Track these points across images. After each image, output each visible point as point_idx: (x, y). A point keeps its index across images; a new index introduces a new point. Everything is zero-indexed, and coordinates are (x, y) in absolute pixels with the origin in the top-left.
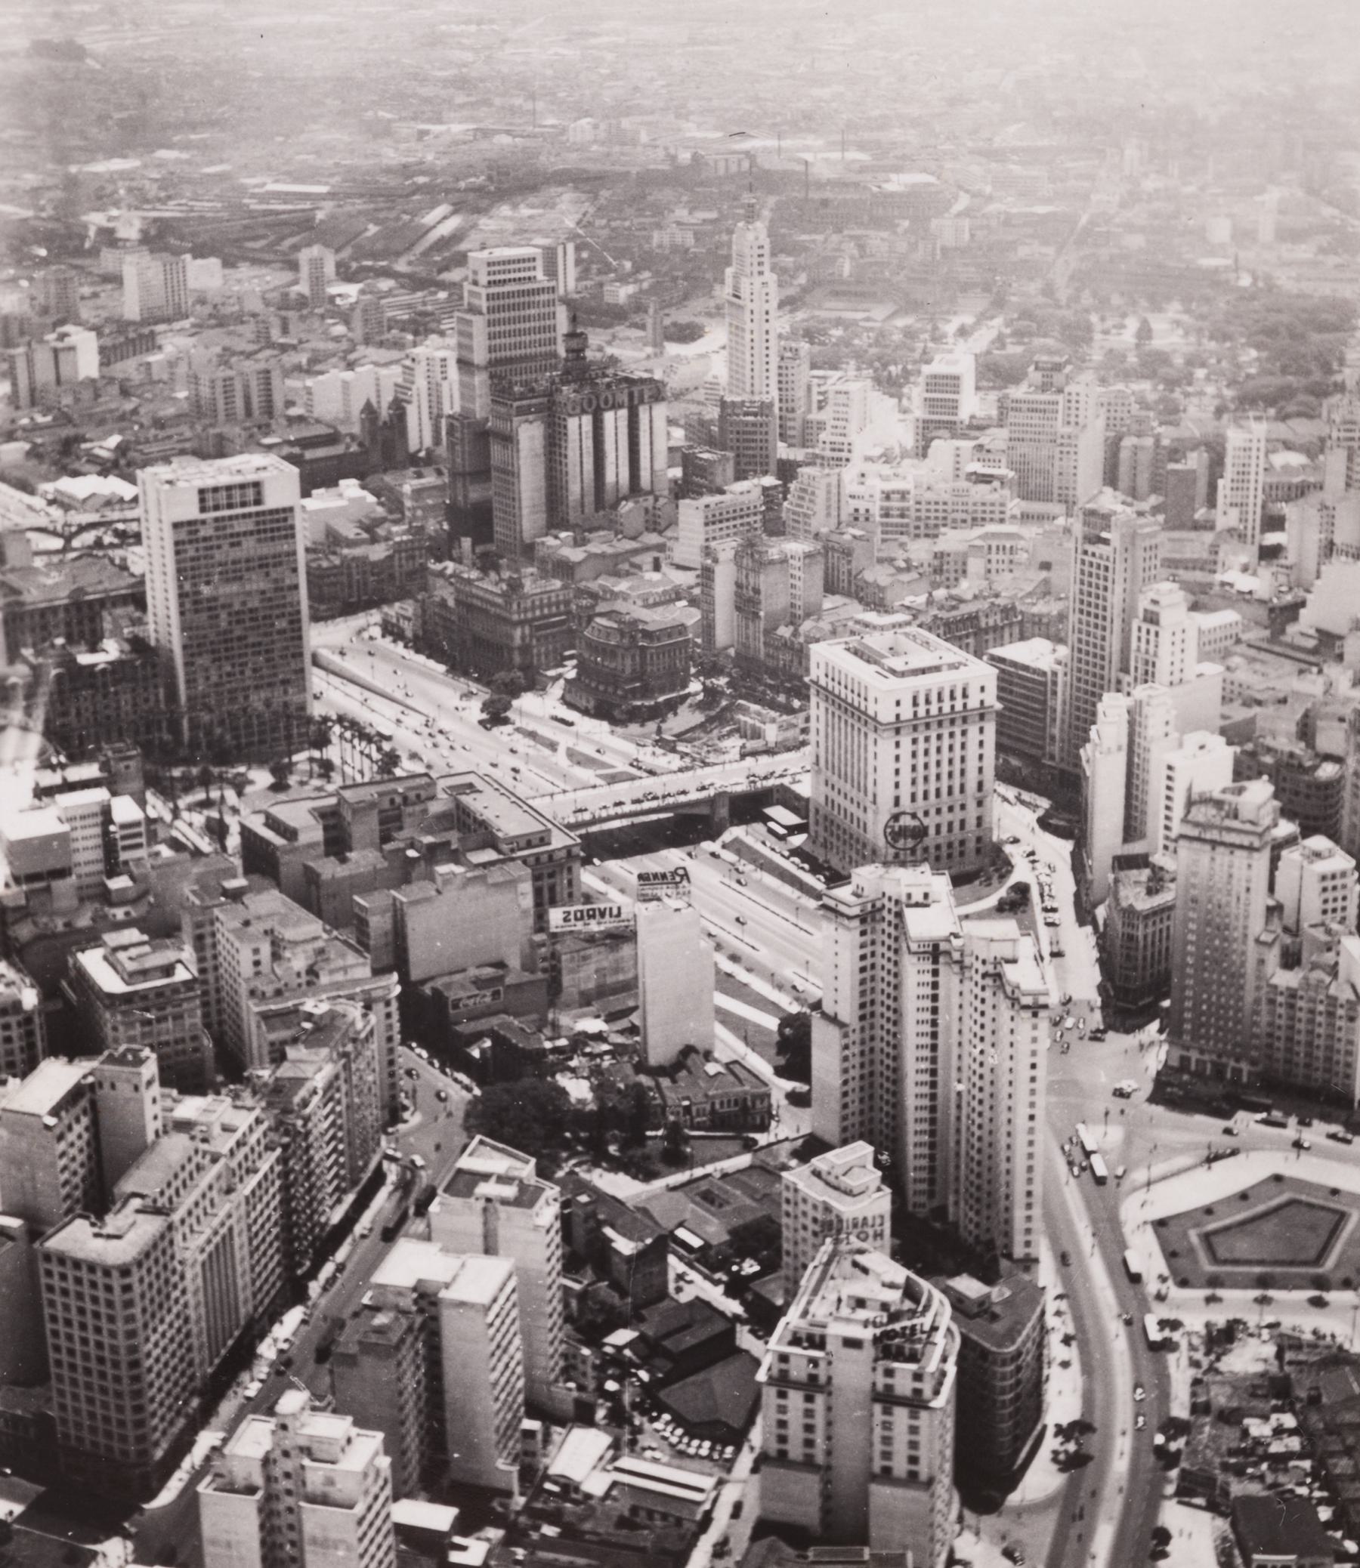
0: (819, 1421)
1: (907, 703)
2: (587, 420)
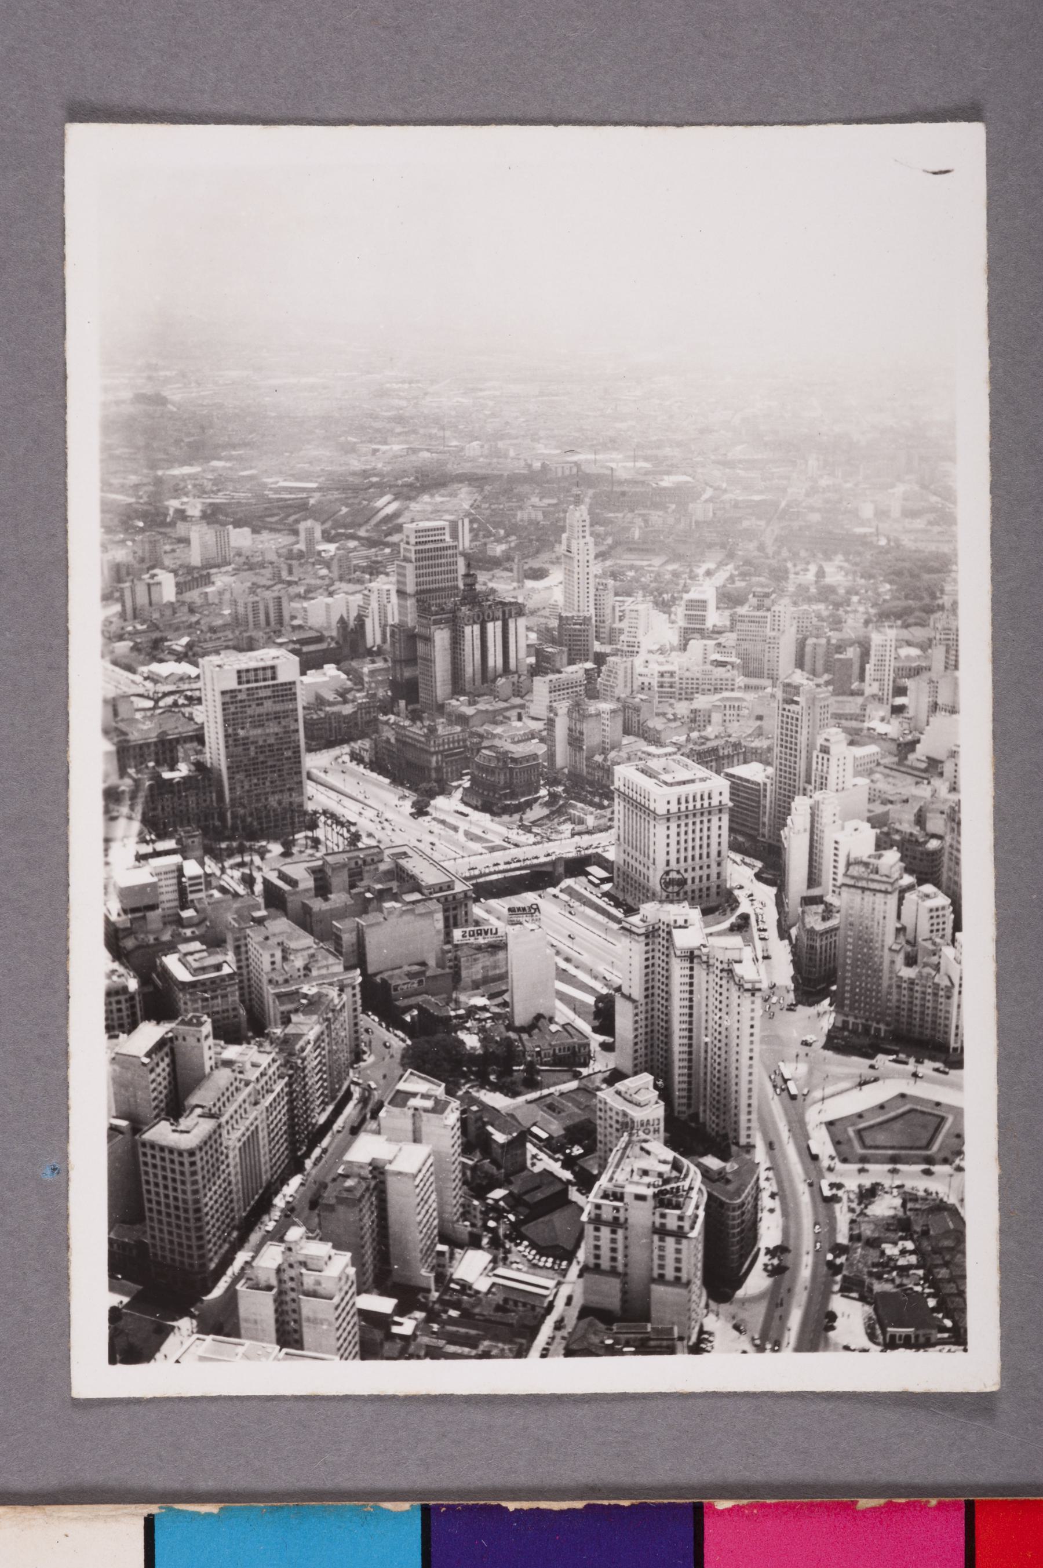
0: (620, 1246)
1: (674, 803)
2: (477, 628)
